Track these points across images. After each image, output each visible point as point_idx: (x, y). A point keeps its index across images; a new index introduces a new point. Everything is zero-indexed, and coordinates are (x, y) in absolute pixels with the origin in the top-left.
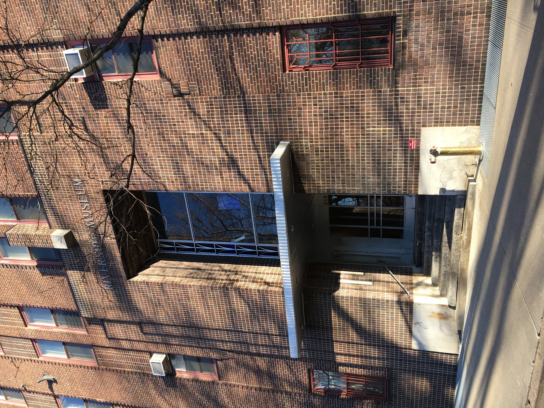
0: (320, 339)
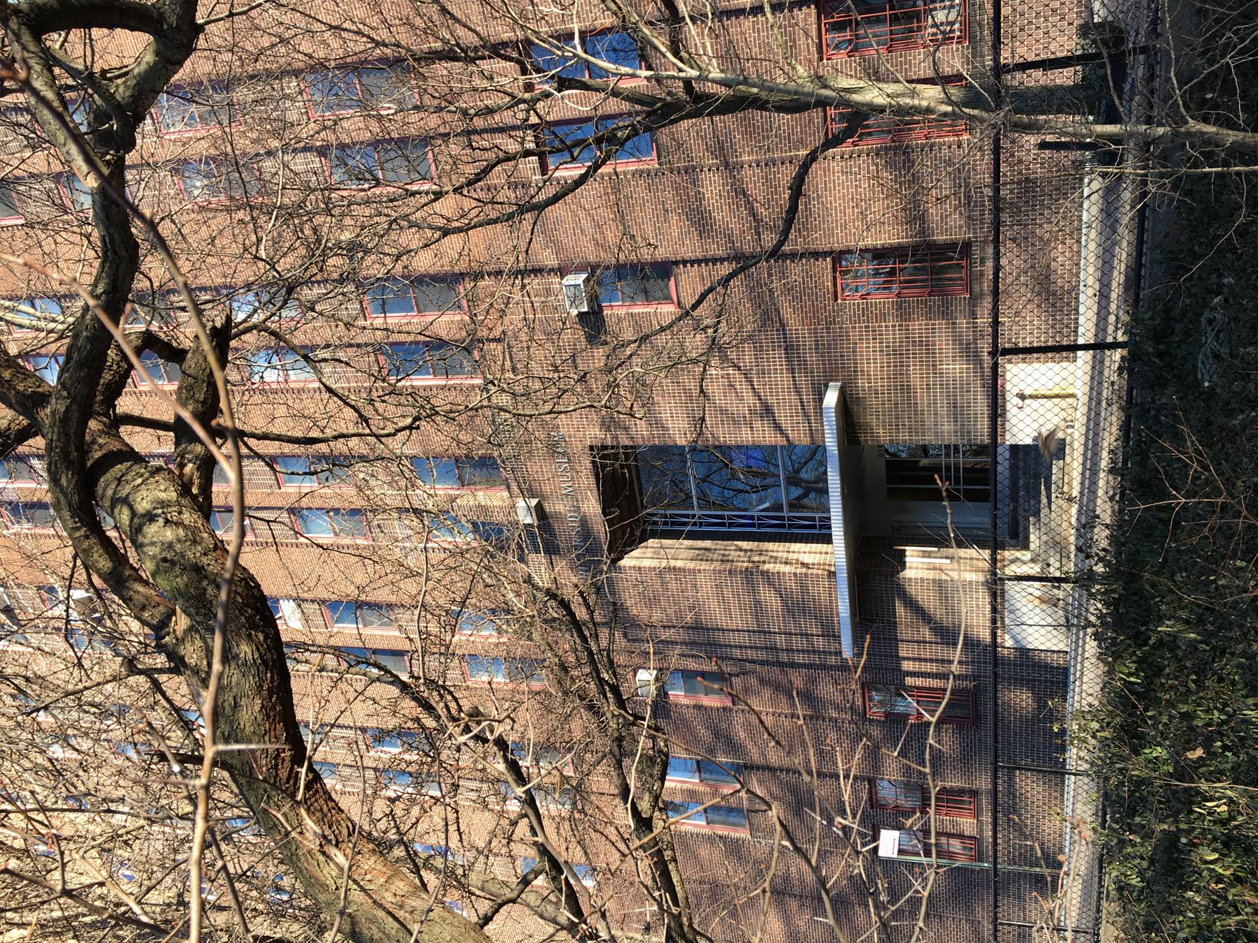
0: (879, 639)
